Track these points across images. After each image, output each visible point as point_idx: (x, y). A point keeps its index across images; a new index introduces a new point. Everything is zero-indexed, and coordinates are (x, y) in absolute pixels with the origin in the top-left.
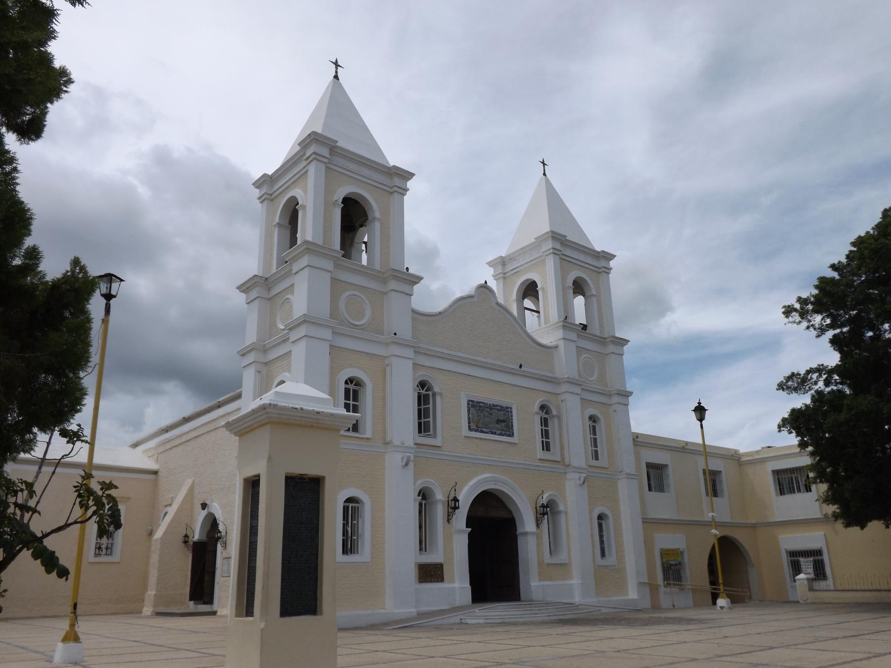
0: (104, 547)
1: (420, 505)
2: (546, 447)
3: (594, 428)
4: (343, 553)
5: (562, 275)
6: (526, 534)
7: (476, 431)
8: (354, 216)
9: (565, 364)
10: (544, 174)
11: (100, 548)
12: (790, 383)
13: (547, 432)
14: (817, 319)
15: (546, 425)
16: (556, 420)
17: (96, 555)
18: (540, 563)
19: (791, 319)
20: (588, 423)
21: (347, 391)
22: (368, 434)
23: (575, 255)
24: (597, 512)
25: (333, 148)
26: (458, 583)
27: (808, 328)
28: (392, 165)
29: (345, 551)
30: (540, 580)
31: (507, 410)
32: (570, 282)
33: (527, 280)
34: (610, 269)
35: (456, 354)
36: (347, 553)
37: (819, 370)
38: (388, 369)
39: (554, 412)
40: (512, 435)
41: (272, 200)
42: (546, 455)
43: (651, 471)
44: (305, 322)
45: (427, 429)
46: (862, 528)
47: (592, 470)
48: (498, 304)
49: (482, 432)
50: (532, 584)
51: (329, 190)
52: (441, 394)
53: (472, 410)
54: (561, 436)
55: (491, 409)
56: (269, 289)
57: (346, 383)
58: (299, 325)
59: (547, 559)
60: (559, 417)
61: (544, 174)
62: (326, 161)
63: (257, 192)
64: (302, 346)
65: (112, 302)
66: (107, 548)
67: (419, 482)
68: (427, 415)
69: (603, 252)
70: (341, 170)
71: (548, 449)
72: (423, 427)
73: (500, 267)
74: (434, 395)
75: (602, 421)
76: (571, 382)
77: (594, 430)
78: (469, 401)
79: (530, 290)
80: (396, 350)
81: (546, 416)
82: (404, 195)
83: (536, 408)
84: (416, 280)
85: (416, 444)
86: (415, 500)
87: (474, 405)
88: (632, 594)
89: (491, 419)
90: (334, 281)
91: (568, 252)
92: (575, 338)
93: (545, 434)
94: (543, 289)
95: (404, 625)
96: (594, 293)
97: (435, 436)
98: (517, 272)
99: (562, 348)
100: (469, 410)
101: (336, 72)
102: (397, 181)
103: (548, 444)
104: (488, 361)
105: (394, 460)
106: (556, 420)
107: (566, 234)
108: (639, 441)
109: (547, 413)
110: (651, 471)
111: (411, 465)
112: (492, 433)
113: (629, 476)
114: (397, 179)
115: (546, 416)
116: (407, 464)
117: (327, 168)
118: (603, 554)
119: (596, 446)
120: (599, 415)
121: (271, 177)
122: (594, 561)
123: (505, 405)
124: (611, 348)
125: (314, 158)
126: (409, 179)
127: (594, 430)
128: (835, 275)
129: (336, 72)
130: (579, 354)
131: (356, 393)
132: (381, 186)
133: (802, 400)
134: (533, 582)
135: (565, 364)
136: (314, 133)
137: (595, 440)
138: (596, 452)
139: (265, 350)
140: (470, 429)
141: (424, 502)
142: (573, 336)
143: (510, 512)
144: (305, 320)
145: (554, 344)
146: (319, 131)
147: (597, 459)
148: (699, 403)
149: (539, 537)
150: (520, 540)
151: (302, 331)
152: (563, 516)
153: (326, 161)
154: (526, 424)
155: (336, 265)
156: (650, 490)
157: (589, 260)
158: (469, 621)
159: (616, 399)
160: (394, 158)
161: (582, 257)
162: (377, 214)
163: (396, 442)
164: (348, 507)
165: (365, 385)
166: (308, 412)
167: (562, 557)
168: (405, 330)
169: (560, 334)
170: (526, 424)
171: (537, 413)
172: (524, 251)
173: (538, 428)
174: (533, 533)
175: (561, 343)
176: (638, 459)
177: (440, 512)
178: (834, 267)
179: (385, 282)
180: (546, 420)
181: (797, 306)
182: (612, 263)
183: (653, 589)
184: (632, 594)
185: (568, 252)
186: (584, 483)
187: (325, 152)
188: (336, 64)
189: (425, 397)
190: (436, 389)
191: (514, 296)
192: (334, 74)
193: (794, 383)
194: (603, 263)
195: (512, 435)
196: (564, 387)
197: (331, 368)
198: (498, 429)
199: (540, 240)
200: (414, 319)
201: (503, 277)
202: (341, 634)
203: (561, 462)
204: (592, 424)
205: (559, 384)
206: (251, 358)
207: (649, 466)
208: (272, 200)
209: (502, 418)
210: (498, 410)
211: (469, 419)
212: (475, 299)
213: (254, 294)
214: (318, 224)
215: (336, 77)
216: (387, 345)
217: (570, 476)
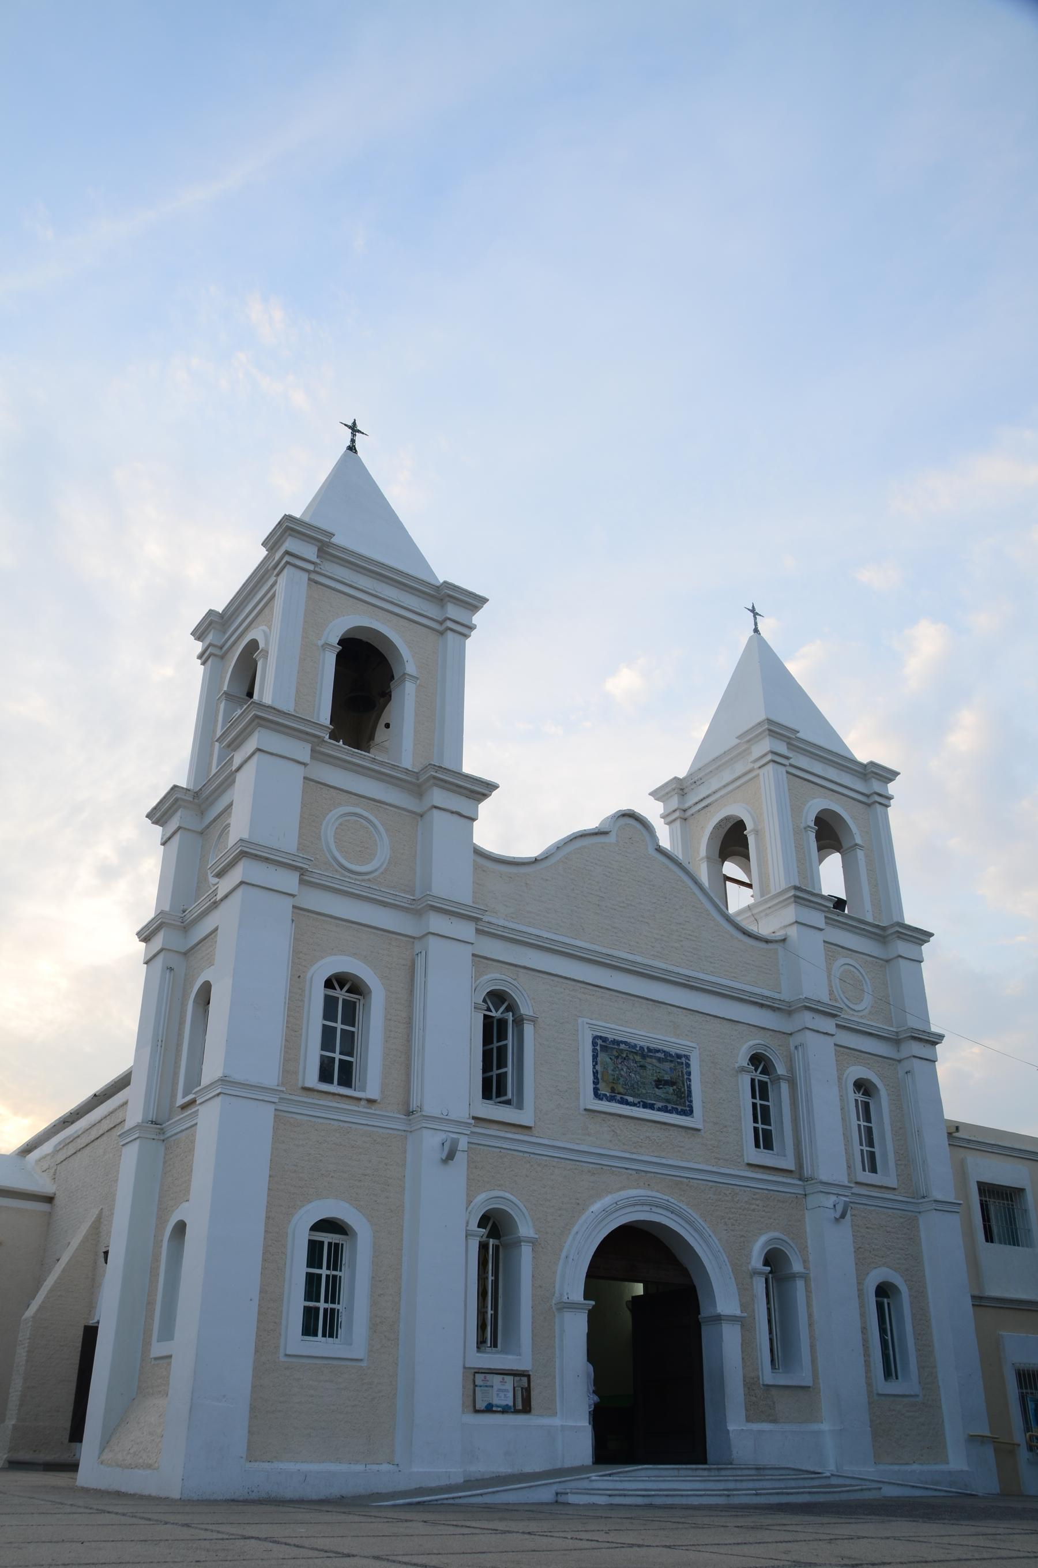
1: (483, 1247)
2: (764, 1140)
3: (866, 1106)
6: (718, 1319)
7: (611, 1099)
13: (765, 1110)
15: (764, 1096)
16: (784, 1087)
18: (751, 1384)
20: (853, 1095)
21: (330, 1005)
22: (372, 1091)
24: (875, 1277)
25: (325, 547)
26: (566, 1423)
28: (441, 581)
30: (749, 1419)
31: (679, 1061)
33: (727, 819)
34: (889, 798)
39: (781, 1070)
40: (689, 1112)
42: (763, 1157)
43: (991, 1201)
44: (243, 854)
45: (501, 1091)
47: (857, 1190)
48: (660, 850)
50: (731, 1427)
52: (534, 1020)
53: (602, 1057)
55: (644, 1057)
56: (202, 813)
57: (328, 984)
59: (768, 1377)
60: (792, 1082)
62: (311, 567)
63: (198, 647)
67: (482, 1197)
68: (502, 1063)
69: (872, 764)
71: (768, 1146)
72: (493, 1087)
74: (519, 1022)
75: (883, 1093)
77: (866, 1112)
78: (595, 1038)
79: (733, 841)
81: (765, 1078)
82: (466, 636)
83: (743, 1060)
84: (480, 790)
85: (474, 1118)
86: (468, 1235)
87: (604, 1046)
88: (956, 1460)
89: (643, 1078)
91: (803, 762)
92: (821, 924)
93: (762, 1114)
94: (757, 832)
95: (426, 1503)
97: (520, 1106)
98: (706, 806)
100: (595, 1057)
101: (353, 441)
102: (453, 611)
103: (768, 1134)
104: (639, 959)
106: (784, 1087)
107: (797, 728)
108: (957, 1136)
110: (991, 1201)
111: (461, 1158)
112: (645, 1106)
113: (943, 1206)
114: (452, 609)
115: (765, 1078)
116: (451, 1156)
118: (888, 1373)
119: (871, 1143)
120: (876, 1080)
121: (221, 616)
122: (869, 1384)
123: (673, 1051)
125: (287, 563)
127: (866, 1112)
129: (353, 441)
130: (830, 959)
134: (738, 1428)
136: (288, 518)
137: (869, 1131)
138: (872, 1156)
139: (186, 927)
141: (491, 1241)
142: (817, 918)
143: (685, 1272)
144: (245, 853)
145: (780, 934)
146: (297, 514)
147: (874, 1170)
149: (745, 1323)
150: (706, 1332)
152: (800, 1284)
153: (311, 567)
154: (720, 1093)
155: (316, 754)
156: (989, 1237)
157: (846, 779)
158: (572, 1499)
160: (446, 568)
161: (832, 773)
162: (410, 668)
165: (370, 992)
167: (803, 1377)
170: (720, 1093)
171: (742, 1070)
174: (733, 1319)
176: (961, 1172)
180: (763, 1086)
182: (892, 788)
183: (1004, 1451)
184: (956, 1460)
185: (803, 762)
186: (843, 1216)
188: (354, 428)
190: (525, 1010)
191: (703, 852)
192: (349, 443)
194: (876, 786)
195: (689, 1112)
197: (296, 952)
198: (658, 1098)
199: (749, 738)
200: (476, 867)
201: (682, 817)
203: (799, 1173)
204: (860, 1097)
207: (986, 1190)
209: (667, 1077)
210: (659, 1060)
211: (595, 1074)
212: (612, 838)
213: (174, 823)
214: (299, 680)
215: (352, 448)
217: (812, 1201)
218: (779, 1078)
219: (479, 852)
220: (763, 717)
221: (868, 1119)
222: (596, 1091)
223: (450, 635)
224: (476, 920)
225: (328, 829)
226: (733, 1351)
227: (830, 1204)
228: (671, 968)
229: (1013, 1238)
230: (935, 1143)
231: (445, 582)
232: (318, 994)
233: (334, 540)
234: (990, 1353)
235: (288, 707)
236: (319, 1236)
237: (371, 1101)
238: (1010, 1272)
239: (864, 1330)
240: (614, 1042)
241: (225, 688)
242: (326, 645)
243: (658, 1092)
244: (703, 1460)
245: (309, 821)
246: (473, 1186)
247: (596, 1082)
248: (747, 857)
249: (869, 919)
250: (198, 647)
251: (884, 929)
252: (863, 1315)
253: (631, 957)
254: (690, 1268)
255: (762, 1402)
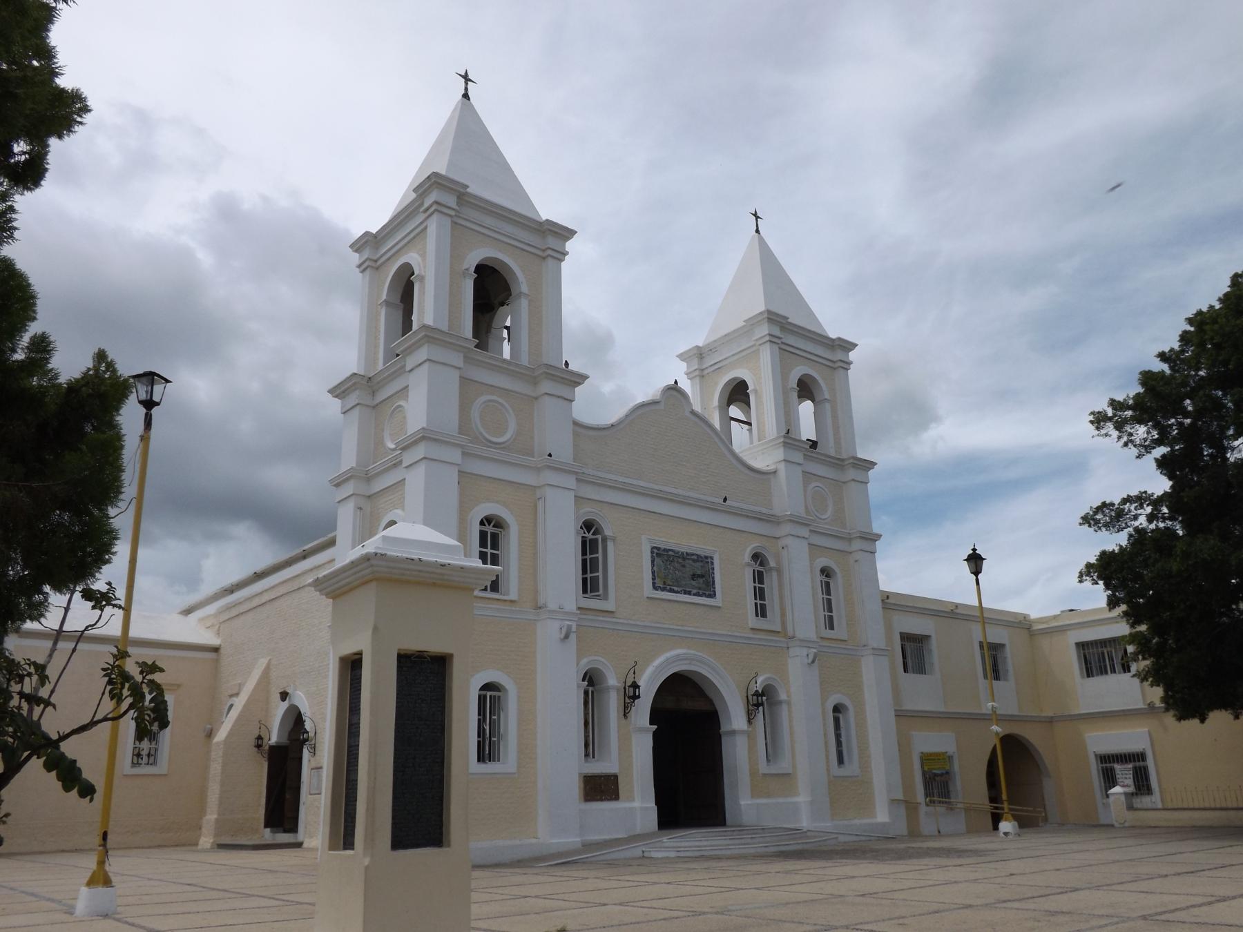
0: (144, 753)
1: (586, 693)
2: (761, 611)
3: (828, 584)
4: (479, 760)
5: (782, 371)
6: (733, 732)
7: (663, 589)
8: (491, 290)
9: (787, 496)
10: (757, 231)
11: (139, 755)
12: (1099, 516)
13: (762, 590)
14: (1141, 431)
15: (761, 581)
16: (775, 574)
17: (134, 765)
18: (753, 773)
19: (1103, 432)
20: (819, 578)
21: (483, 535)
22: (513, 595)
23: (801, 344)
25: (462, 195)
26: (639, 801)
27: (1126, 444)
29: (481, 758)
31: (706, 561)
32: (793, 383)
33: (734, 379)
34: (849, 363)
35: (635, 482)
36: (484, 761)
37: (1141, 499)
38: (540, 504)
39: (772, 564)
40: (713, 595)
41: (377, 269)
43: (908, 645)
44: (423, 438)
45: (595, 588)
46: (1203, 721)
47: (826, 643)
48: (693, 412)
49: (671, 591)
50: (742, 803)
51: (456, 255)
52: (614, 539)
53: (657, 560)
54: (781, 597)
55: (684, 559)
56: (374, 394)
57: (482, 523)
58: (415, 443)
59: (763, 767)
60: (779, 571)
61: (757, 231)
62: (453, 213)
63: (356, 258)
64: (421, 470)
65: (155, 411)
66: (149, 755)
67: (585, 661)
68: (594, 568)
69: (839, 339)
70: (468, 224)
71: (764, 615)
72: (590, 585)
73: (696, 361)
74: (605, 540)
75: (839, 575)
76: (795, 521)
77: (827, 588)
79: (738, 393)
80: (550, 477)
81: (761, 569)
82: (561, 260)
83: (747, 558)
86: (578, 686)
87: (659, 553)
88: (882, 815)
89: (684, 573)
90: (465, 381)
91: (791, 340)
93: (760, 594)
96: (827, 396)
97: (606, 597)
98: (719, 368)
99: (782, 473)
100: (653, 562)
101: (466, 89)
102: (552, 242)
103: (763, 607)
104: (680, 492)
105: (548, 631)
106: (775, 574)
108: (890, 603)
109: (761, 564)
110: (908, 645)
111: (573, 637)
113: (877, 652)
114: (552, 238)
115: (761, 569)
116: (567, 637)
117: (454, 223)
118: (841, 761)
119: (830, 610)
121: (375, 236)
122: (828, 770)
123: (703, 554)
124: (852, 473)
126: (568, 239)
127: (827, 588)
128: (1165, 367)
131: (495, 537)
132: (412, 235)
133: (1116, 541)
134: (743, 799)
135: (787, 496)
136: (435, 174)
137: (829, 601)
138: (831, 618)
139: (368, 478)
140: (655, 588)
141: (591, 689)
142: (798, 457)
143: (711, 702)
144: (424, 437)
145: (772, 467)
146: (443, 172)
147: (832, 628)
148: (974, 550)
149: (751, 736)
151: (420, 451)
152: (785, 707)
153: (453, 213)
154: (732, 579)
156: (906, 671)
157: (819, 351)
159: (857, 545)
160: (548, 209)
161: (810, 347)
162: (524, 288)
163: (552, 606)
164: (485, 696)
166: (429, 564)
167: (783, 766)
168: (564, 451)
169: (779, 454)
170: (732, 579)
171: (748, 565)
172: (729, 338)
173: (749, 585)
175: (782, 467)
176: (889, 627)
177: (613, 702)
178: (1163, 356)
179: (534, 381)
180: (760, 574)
181: (1110, 413)
182: (852, 355)
183: (911, 807)
184: (882, 815)
185: (791, 340)
186: (813, 662)
187: (451, 201)
188: (466, 78)
189: (591, 543)
190: (608, 532)
193: (1105, 516)
194: (839, 355)
195: (713, 595)
196: (786, 529)
198: (694, 587)
199: (752, 323)
200: (576, 434)
201: (701, 375)
202: (476, 873)
203: (782, 633)
204: (825, 579)
205: (779, 523)
206: (348, 489)
207: (906, 638)
208: (377, 269)
210: (694, 561)
211: (653, 573)
212: (662, 406)
213: (353, 399)
214: (441, 302)
215: (466, 96)
216: (538, 470)
217: (793, 652)
218: (771, 569)
219: (576, 423)
220: (762, 308)
221: (828, 593)
222: (654, 584)
223: (550, 261)
224: (576, 473)
225: (475, 414)
226: (741, 749)
227: (805, 653)
228: (702, 497)
229: (921, 668)
230: (876, 607)
231: (547, 220)
232: (476, 530)
233: (468, 190)
234: (904, 746)
235: (445, 328)
236: (483, 693)
237: (512, 601)
238: (923, 693)
239: (825, 735)
240: (665, 550)
241: (384, 297)
242: (465, 273)
243: (694, 583)
244: (722, 823)
245: (464, 408)
246: (580, 654)
247: (654, 579)
248: (748, 404)
249: (833, 454)
250: (356, 258)
251: (843, 460)
252: (825, 725)
253: (675, 491)
254: (711, 695)
255: (762, 785)
